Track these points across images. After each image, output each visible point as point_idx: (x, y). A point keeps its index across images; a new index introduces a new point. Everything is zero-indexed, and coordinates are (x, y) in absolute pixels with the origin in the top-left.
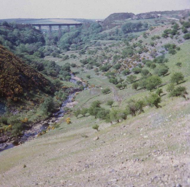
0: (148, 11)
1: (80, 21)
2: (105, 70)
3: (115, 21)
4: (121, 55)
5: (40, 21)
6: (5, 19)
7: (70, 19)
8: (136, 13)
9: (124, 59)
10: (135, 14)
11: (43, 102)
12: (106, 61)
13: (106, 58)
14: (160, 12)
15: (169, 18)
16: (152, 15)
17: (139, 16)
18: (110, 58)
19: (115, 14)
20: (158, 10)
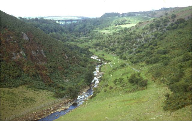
0: (129, 12)
1: (77, 17)
2: (113, 50)
3: (108, 18)
4: (123, 40)
5: (53, 18)
6: (97, 18)
7: (74, 17)
8: (121, 13)
9: (125, 43)
10: (121, 14)
11: (163, 80)
12: (112, 44)
13: (111, 42)
14: (136, 13)
15: (146, 17)
16: (132, 14)
17: (123, 15)
18: (114, 42)
19: (107, 13)
20: (135, 11)
